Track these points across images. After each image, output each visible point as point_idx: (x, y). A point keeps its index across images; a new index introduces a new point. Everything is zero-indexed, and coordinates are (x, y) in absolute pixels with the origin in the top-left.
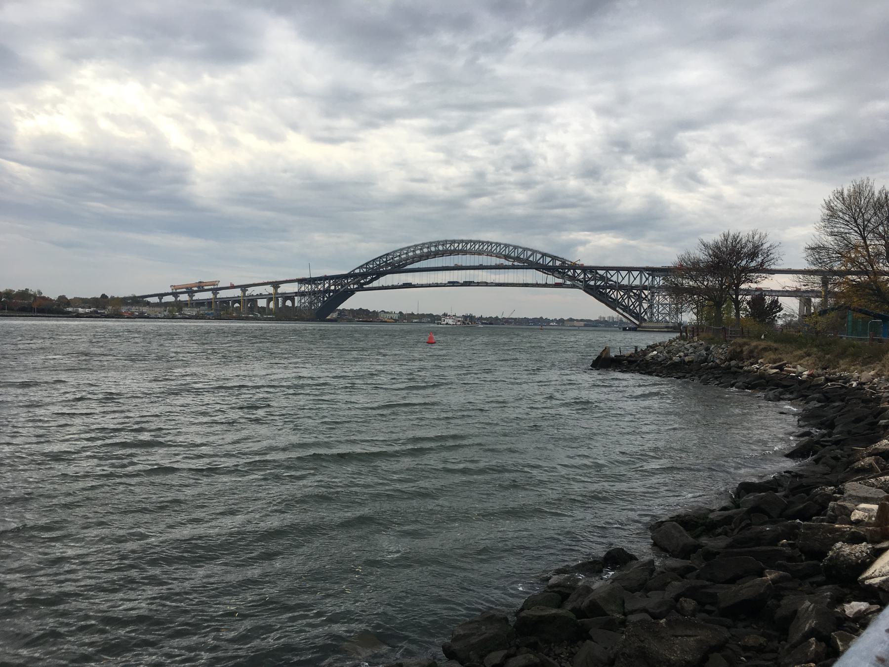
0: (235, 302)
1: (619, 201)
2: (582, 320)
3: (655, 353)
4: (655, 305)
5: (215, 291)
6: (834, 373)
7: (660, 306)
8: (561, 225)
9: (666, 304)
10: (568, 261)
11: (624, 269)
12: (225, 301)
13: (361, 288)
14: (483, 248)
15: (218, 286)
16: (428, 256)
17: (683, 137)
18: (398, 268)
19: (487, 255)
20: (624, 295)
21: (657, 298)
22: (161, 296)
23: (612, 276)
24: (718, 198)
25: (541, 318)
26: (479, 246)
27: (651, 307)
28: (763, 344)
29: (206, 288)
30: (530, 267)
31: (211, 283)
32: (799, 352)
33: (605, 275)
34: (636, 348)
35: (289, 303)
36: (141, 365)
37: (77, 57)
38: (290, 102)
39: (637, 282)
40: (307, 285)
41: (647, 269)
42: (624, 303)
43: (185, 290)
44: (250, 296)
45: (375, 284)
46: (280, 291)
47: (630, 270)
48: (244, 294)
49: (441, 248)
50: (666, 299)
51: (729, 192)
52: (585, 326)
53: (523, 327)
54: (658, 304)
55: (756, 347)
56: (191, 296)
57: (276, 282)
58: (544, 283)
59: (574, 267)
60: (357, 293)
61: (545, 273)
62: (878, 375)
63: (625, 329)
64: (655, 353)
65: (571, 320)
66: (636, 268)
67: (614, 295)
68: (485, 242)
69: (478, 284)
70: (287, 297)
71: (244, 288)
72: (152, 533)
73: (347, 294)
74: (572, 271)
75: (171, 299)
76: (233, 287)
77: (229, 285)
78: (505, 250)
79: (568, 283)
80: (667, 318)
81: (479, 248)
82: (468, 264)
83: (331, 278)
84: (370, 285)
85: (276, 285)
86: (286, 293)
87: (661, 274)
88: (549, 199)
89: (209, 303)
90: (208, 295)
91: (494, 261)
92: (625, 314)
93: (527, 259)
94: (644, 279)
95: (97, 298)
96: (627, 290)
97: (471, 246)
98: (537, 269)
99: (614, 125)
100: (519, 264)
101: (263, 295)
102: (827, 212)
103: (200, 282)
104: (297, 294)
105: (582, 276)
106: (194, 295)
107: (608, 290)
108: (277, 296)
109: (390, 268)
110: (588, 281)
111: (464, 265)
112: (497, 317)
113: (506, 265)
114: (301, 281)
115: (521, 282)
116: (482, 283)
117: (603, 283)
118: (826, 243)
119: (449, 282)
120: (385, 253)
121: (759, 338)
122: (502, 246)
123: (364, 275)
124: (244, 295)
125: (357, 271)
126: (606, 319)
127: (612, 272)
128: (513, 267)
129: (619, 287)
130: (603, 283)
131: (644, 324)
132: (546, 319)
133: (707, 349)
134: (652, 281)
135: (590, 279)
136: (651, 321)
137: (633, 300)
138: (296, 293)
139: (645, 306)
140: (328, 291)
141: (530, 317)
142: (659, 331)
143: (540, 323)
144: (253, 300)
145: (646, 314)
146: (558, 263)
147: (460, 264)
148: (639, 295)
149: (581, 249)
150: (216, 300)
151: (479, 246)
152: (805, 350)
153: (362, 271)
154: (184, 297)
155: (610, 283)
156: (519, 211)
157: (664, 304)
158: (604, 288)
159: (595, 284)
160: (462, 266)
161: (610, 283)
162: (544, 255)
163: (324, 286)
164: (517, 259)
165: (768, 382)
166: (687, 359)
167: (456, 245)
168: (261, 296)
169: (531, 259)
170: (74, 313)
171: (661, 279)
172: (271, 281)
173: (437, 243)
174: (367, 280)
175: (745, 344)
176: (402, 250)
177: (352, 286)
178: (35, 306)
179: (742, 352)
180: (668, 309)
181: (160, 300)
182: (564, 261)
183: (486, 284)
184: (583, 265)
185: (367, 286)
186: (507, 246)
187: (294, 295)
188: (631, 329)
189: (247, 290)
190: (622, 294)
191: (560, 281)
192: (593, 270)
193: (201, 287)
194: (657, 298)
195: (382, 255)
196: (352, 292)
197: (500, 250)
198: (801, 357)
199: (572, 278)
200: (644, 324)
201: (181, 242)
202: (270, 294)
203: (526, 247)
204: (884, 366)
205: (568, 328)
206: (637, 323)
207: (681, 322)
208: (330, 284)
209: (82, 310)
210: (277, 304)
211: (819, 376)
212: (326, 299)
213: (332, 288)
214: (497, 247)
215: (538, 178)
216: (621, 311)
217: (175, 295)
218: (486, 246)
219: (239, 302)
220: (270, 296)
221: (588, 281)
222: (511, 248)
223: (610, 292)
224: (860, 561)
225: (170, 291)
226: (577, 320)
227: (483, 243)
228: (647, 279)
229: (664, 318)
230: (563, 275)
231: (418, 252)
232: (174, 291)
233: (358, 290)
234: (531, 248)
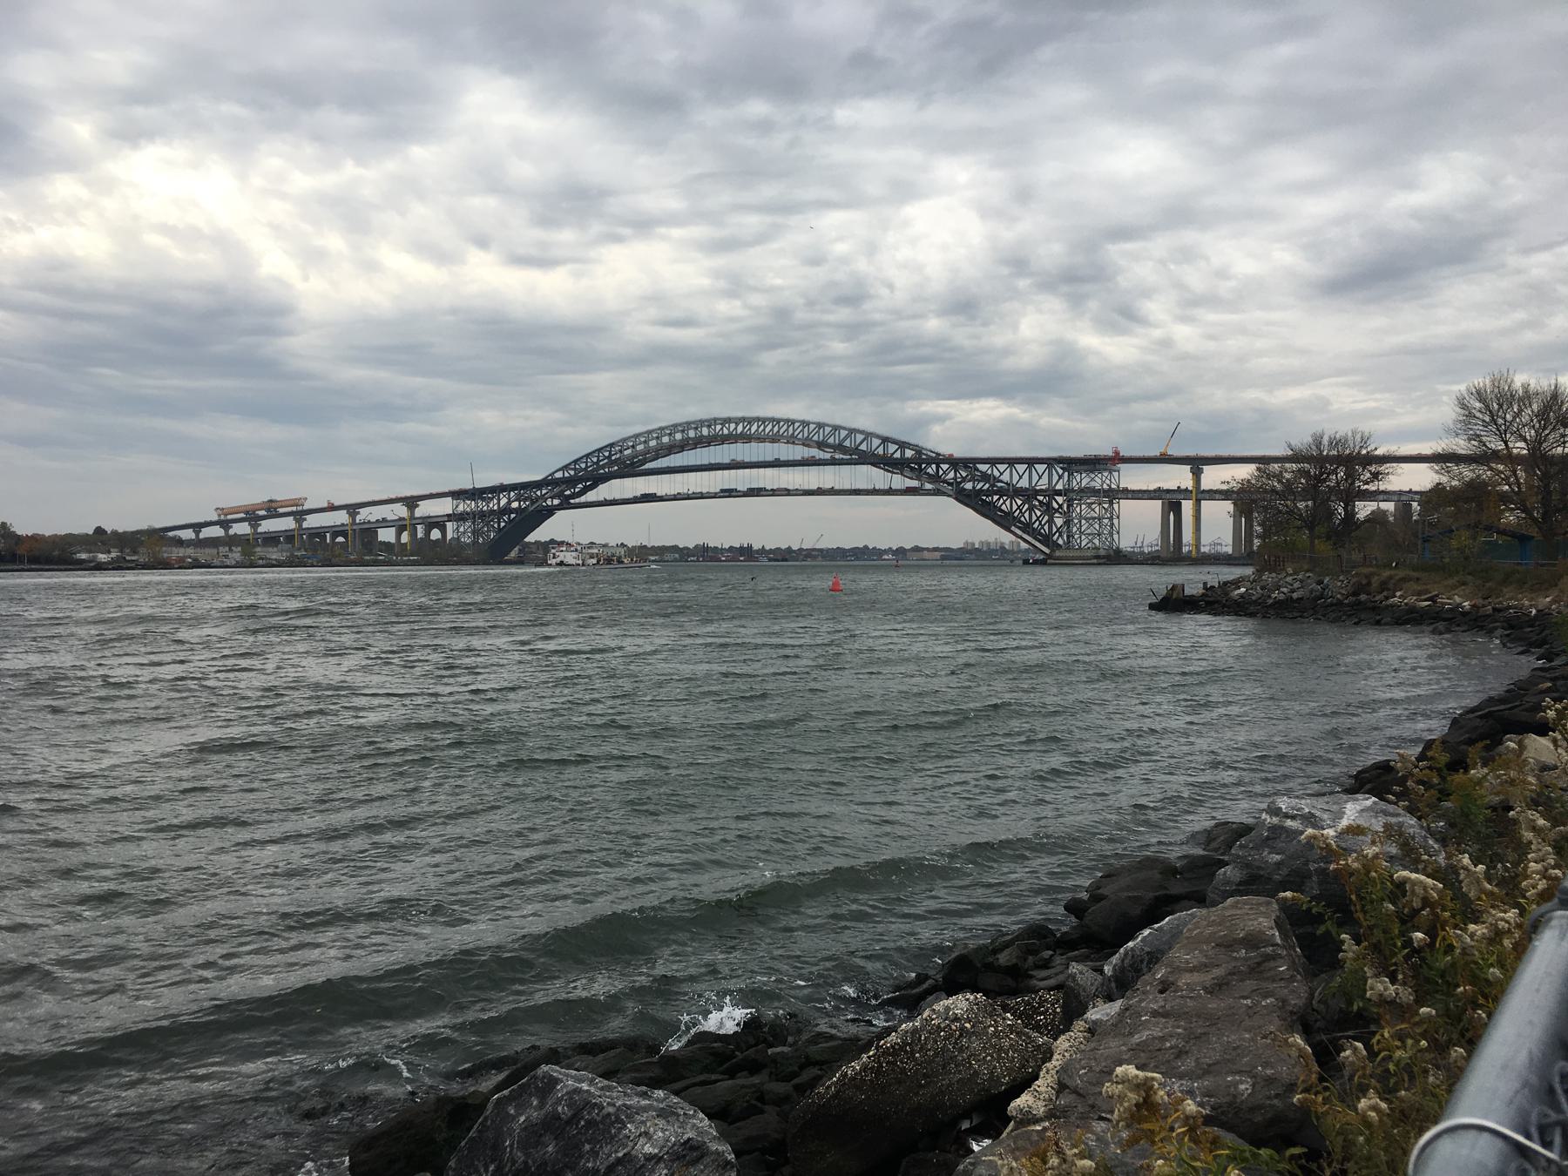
0: (335, 534)
1: (1007, 352)
2: (936, 549)
3: (1243, 590)
4: (1076, 521)
5: (300, 515)
6: (1501, 603)
7: (1083, 522)
8: (905, 390)
9: (1094, 518)
10: (926, 449)
11: (1041, 461)
12: (318, 533)
13: (566, 505)
14: (764, 430)
15: (305, 508)
16: (682, 447)
17: (1115, 251)
18: (630, 468)
19: (788, 442)
20: (1023, 504)
21: (1078, 509)
22: (197, 527)
23: (1001, 474)
24: (1166, 343)
25: (866, 547)
26: (759, 427)
27: (1068, 523)
28: (1401, 574)
29: (281, 510)
30: (862, 461)
31: (292, 502)
32: (1450, 582)
33: (989, 472)
34: (1205, 584)
35: (436, 534)
37: (131, 135)
38: (484, 205)
39: (1043, 484)
40: (469, 502)
41: (1060, 460)
42: (1022, 519)
43: (242, 515)
44: (364, 523)
45: (591, 496)
46: (419, 513)
47: (1031, 462)
48: (354, 520)
49: (705, 431)
50: (1093, 510)
51: (1185, 335)
52: (943, 558)
53: (839, 563)
54: (1080, 517)
55: (1391, 577)
56: (255, 526)
57: (412, 497)
58: (887, 487)
59: (938, 460)
61: (889, 471)
62: (1554, 601)
63: (1026, 562)
64: (1243, 590)
65: (917, 549)
66: (1043, 459)
68: (783, 420)
69: (774, 493)
70: (432, 523)
71: (352, 509)
74: (934, 466)
75: (217, 532)
76: (332, 508)
77: (326, 505)
78: (802, 431)
79: (928, 486)
80: (1096, 541)
81: (757, 430)
82: (754, 459)
83: (513, 487)
84: (583, 499)
85: (411, 502)
86: (430, 517)
87: (1082, 467)
88: (891, 350)
89: (289, 537)
90: (288, 524)
91: (799, 452)
93: (857, 448)
94: (1055, 477)
95: (87, 535)
96: (1028, 496)
97: (744, 428)
98: (874, 464)
99: (1009, 235)
100: (841, 456)
101: (387, 521)
102: (1463, 412)
103: (271, 501)
104: (450, 517)
105: (952, 475)
106: (260, 525)
107: (996, 498)
108: (414, 522)
109: (616, 468)
110: (961, 483)
111: (747, 460)
112: (789, 548)
113: (820, 459)
114: (457, 495)
115: (847, 486)
116: (778, 490)
117: (987, 485)
118: (1455, 447)
119: (723, 491)
121: (1388, 566)
122: (812, 427)
123: (570, 482)
125: (559, 475)
126: (977, 546)
127: (1002, 467)
128: (833, 462)
129: (1013, 492)
130: (987, 485)
131: (1058, 553)
132: (696, 546)
133: (1320, 582)
134: (1069, 480)
135: (964, 479)
137: (1039, 513)
138: (448, 515)
139: (1059, 521)
140: (507, 510)
142: (1082, 564)
143: (863, 557)
144: (369, 531)
145: (1060, 535)
146: (909, 453)
147: (739, 459)
148: (1049, 505)
149: (937, 429)
150: (302, 532)
151: (759, 427)
152: (1456, 578)
153: (567, 475)
154: (242, 529)
155: (999, 484)
156: (840, 370)
157: (1090, 519)
158: (989, 493)
159: (974, 487)
160: (744, 463)
161: (999, 484)
162: (885, 440)
163: (499, 503)
164: (839, 447)
165: (1422, 616)
166: (1295, 595)
167: (733, 426)
168: (384, 523)
169: (863, 447)
170: (91, 561)
171: (1083, 475)
172: (403, 495)
173: (700, 424)
174: (577, 490)
175: (1372, 574)
176: (637, 436)
177: (549, 502)
178: (21, 551)
179: (1369, 584)
180: (1097, 526)
181: (197, 535)
182: (919, 451)
183: (787, 492)
185: (577, 500)
186: (820, 426)
187: (446, 519)
188: (1036, 562)
189: (359, 513)
190: (1019, 502)
191: (915, 484)
192: (968, 463)
193: (272, 510)
194: (1078, 509)
195: (568, 462)
196: (550, 512)
197: (794, 431)
198: (1454, 587)
199: (935, 478)
200: (1058, 553)
201: (237, 430)
202: (401, 519)
203: (853, 427)
204: (1562, 591)
205: (912, 562)
206: (1047, 550)
207: (1118, 548)
208: (509, 499)
209: (104, 556)
210: (414, 533)
211: (1484, 606)
212: (503, 524)
213: (515, 505)
214: (788, 427)
215: (877, 317)
216: (1019, 532)
217: (225, 524)
218: (770, 427)
219: (344, 534)
220: (401, 523)
221: (961, 483)
222: (828, 429)
223: (999, 499)
225: (215, 518)
226: (928, 549)
227: (778, 422)
228: (1060, 477)
229: (1091, 541)
230: (919, 473)
231: (665, 440)
232: (222, 517)
233: (560, 507)
234: (861, 428)
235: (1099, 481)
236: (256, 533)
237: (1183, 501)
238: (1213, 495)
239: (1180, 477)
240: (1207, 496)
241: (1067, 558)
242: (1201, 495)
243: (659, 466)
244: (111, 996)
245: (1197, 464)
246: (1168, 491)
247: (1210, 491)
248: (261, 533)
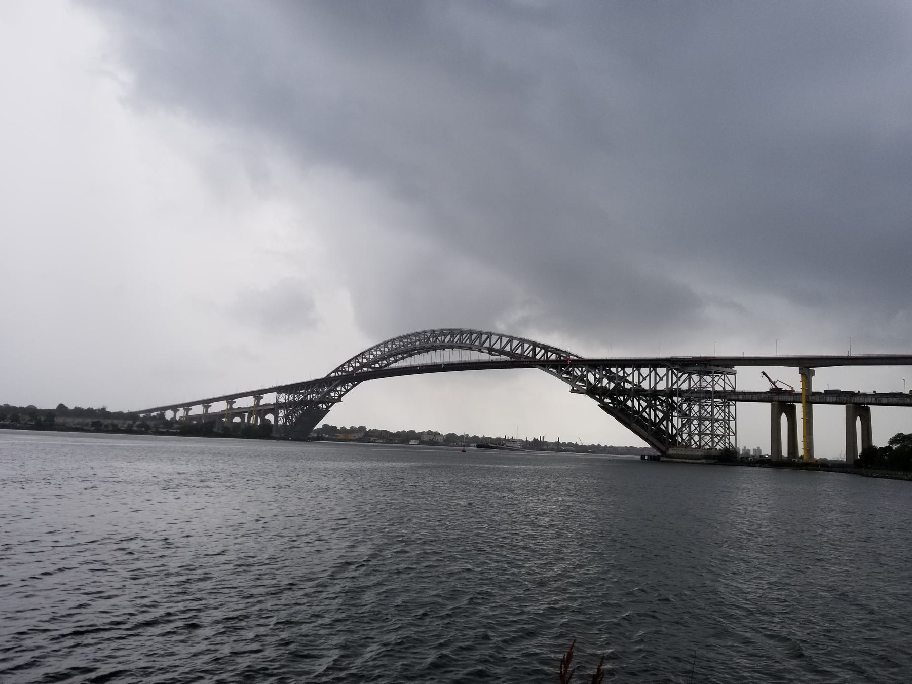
22: (258, 394)
36: (16, 442)
39: (661, 386)
67: (634, 403)
70: (240, 413)
120: (361, 352)
125: (333, 375)
126: (752, 453)
129: (638, 392)
142: (692, 463)
150: (259, 408)
195: (352, 357)
235: (719, 384)
237: (871, 407)
240: (817, 399)
241: (679, 457)
242: (812, 398)
247: (744, 393)
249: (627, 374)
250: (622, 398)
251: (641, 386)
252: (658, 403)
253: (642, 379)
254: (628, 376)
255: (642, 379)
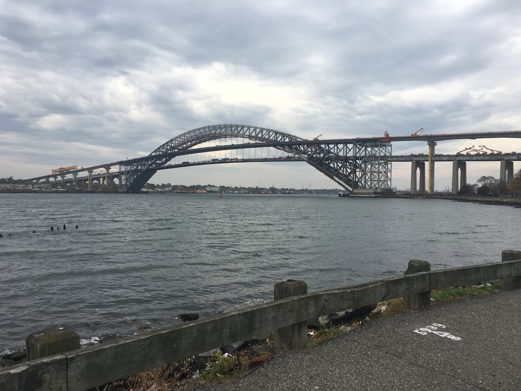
5: (76, 172)
10: (299, 138)
13: (160, 167)
39: (350, 154)
47: (346, 142)
48: (91, 174)
56: (63, 177)
57: (107, 165)
60: (158, 171)
69: (194, 164)
71: (90, 170)
72: (25, 277)
73: (151, 172)
92: (340, 181)
123: (159, 157)
124: (91, 175)
125: (154, 154)
129: (337, 158)
131: (355, 191)
136: (365, 188)
141: (26, 179)
153: (156, 154)
162: (276, 133)
172: (104, 164)
184: (307, 140)
192: (316, 143)
206: (351, 189)
207: (390, 188)
224: (343, 323)
225: (51, 174)
232: (54, 173)
236: (64, 180)
238: (441, 158)
239: (423, 148)
240: (437, 158)
243: (197, 148)
244: (331, 268)
245: (432, 140)
246: (416, 156)
248: (58, 181)
249: (330, 148)
250: (327, 162)
251: (338, 155)
252: (348, 164)
253: (339, 151)
254: (331, 149)
255: (339, 151)
